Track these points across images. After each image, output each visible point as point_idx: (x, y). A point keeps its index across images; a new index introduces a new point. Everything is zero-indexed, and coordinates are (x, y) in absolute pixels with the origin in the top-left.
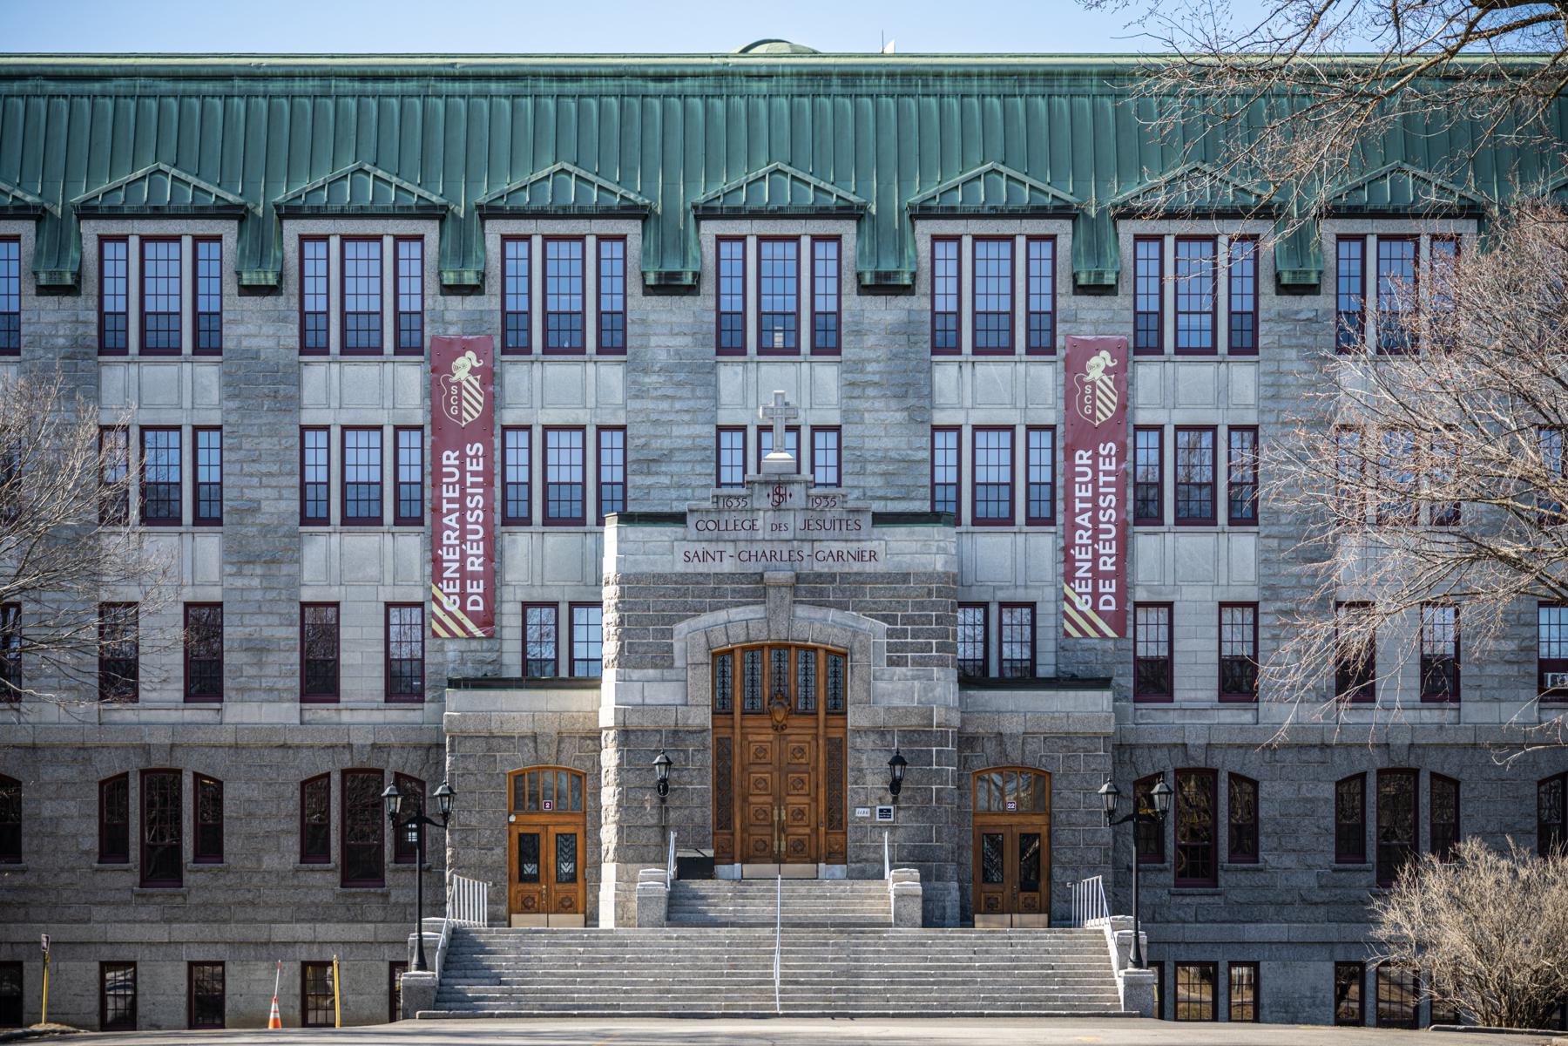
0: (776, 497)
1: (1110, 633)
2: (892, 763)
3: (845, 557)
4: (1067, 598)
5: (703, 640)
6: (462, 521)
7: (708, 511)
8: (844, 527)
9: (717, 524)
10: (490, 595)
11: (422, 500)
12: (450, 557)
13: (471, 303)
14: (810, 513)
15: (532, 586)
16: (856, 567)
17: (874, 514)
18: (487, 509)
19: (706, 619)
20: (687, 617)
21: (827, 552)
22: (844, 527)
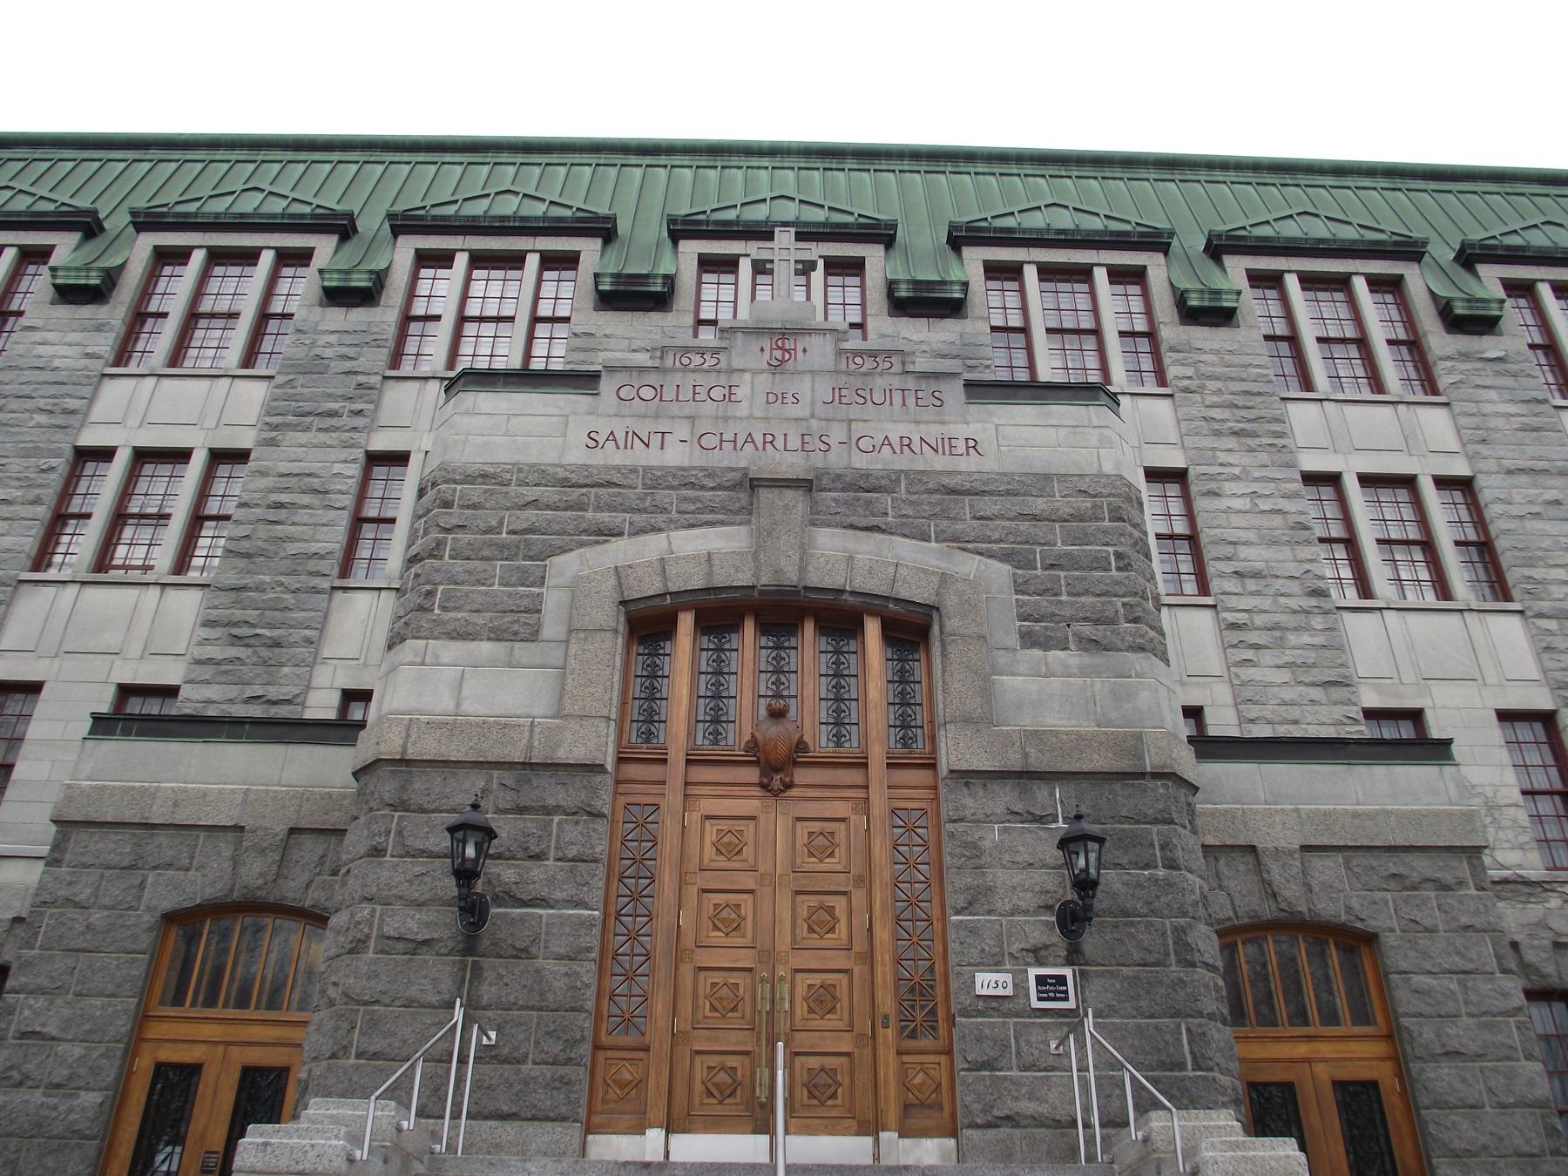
0: (778, 354)
2: (1067, 843)
3: (916, 446)
5: (612, 581)
7: (642, 369)
8: (911, 401)
9: (659, 391)
13: (358, 316)
14: (844, 378)
15: (365, 665)
16: (939, 463)
17: (970, 385)
19: (620, 551)
20: (582, 544)
21: (880, 438)
22: (911, 401)
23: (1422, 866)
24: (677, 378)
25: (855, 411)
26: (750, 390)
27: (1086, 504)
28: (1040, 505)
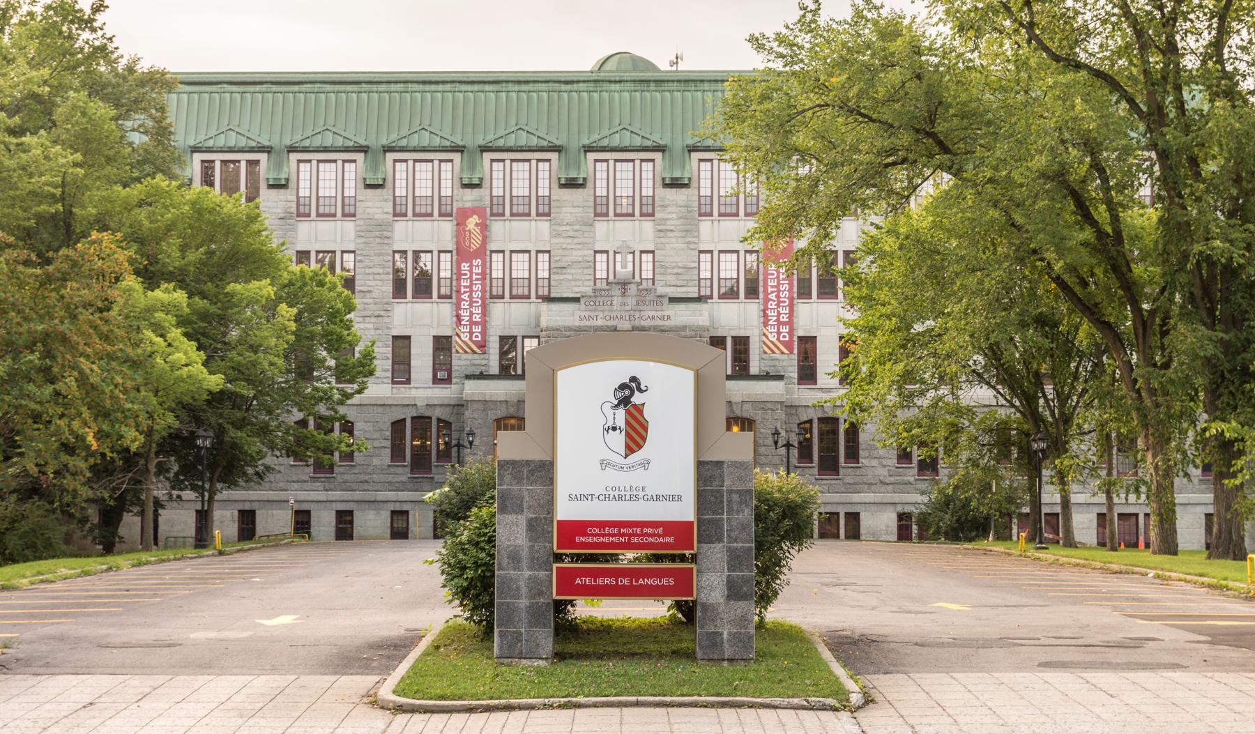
1: (785, 351)
4: (764, 335)
6: (470, 297)
7: (590, 297)
10: (484, 333)
11: (451, 287)
12: (465, 314)
16: (660, 323)
18: (483, 291)
23: (769, 406)
24: (599, 299)
25: (642, 308)
26: (617, 301)
27: (693, 333)
28: (683, 333)
